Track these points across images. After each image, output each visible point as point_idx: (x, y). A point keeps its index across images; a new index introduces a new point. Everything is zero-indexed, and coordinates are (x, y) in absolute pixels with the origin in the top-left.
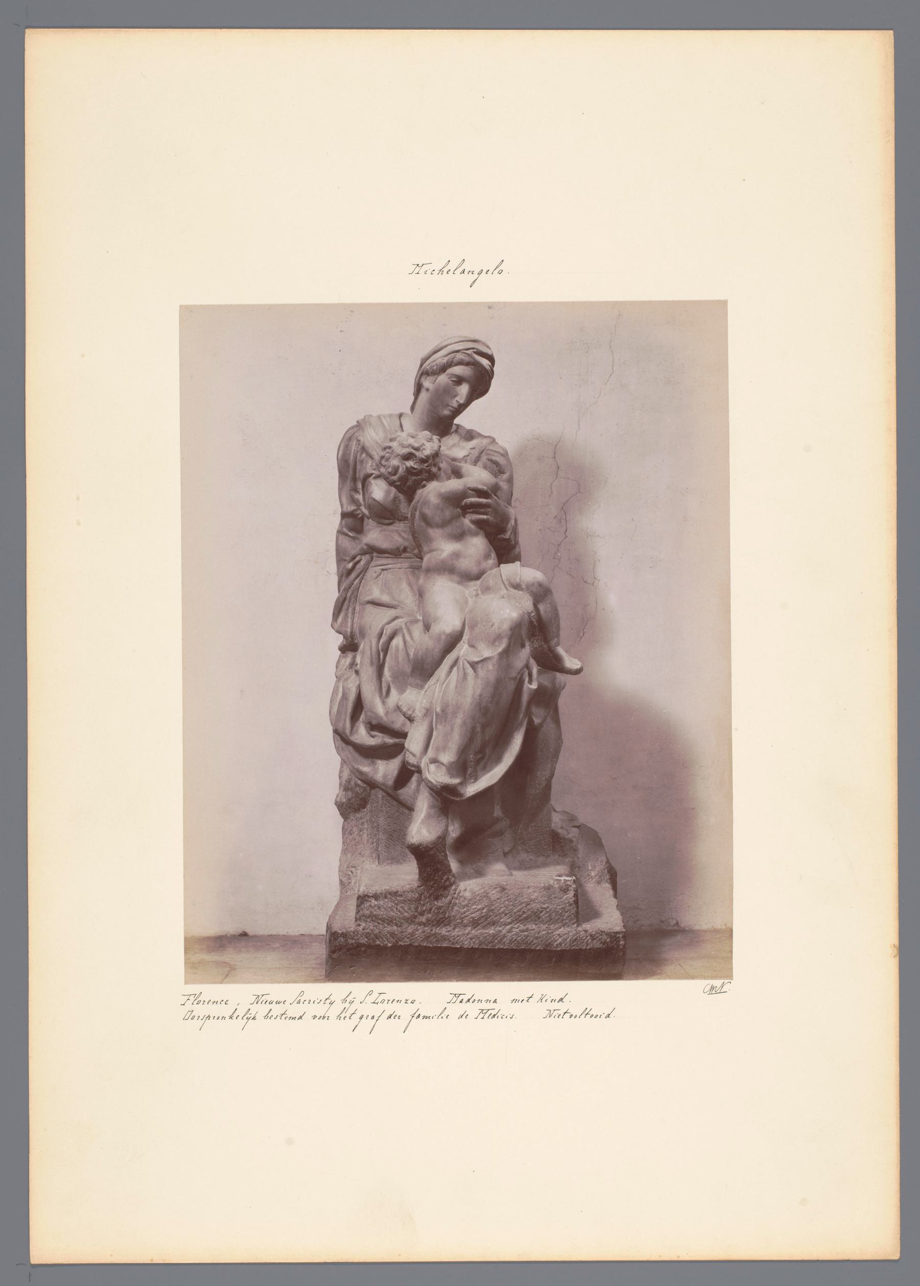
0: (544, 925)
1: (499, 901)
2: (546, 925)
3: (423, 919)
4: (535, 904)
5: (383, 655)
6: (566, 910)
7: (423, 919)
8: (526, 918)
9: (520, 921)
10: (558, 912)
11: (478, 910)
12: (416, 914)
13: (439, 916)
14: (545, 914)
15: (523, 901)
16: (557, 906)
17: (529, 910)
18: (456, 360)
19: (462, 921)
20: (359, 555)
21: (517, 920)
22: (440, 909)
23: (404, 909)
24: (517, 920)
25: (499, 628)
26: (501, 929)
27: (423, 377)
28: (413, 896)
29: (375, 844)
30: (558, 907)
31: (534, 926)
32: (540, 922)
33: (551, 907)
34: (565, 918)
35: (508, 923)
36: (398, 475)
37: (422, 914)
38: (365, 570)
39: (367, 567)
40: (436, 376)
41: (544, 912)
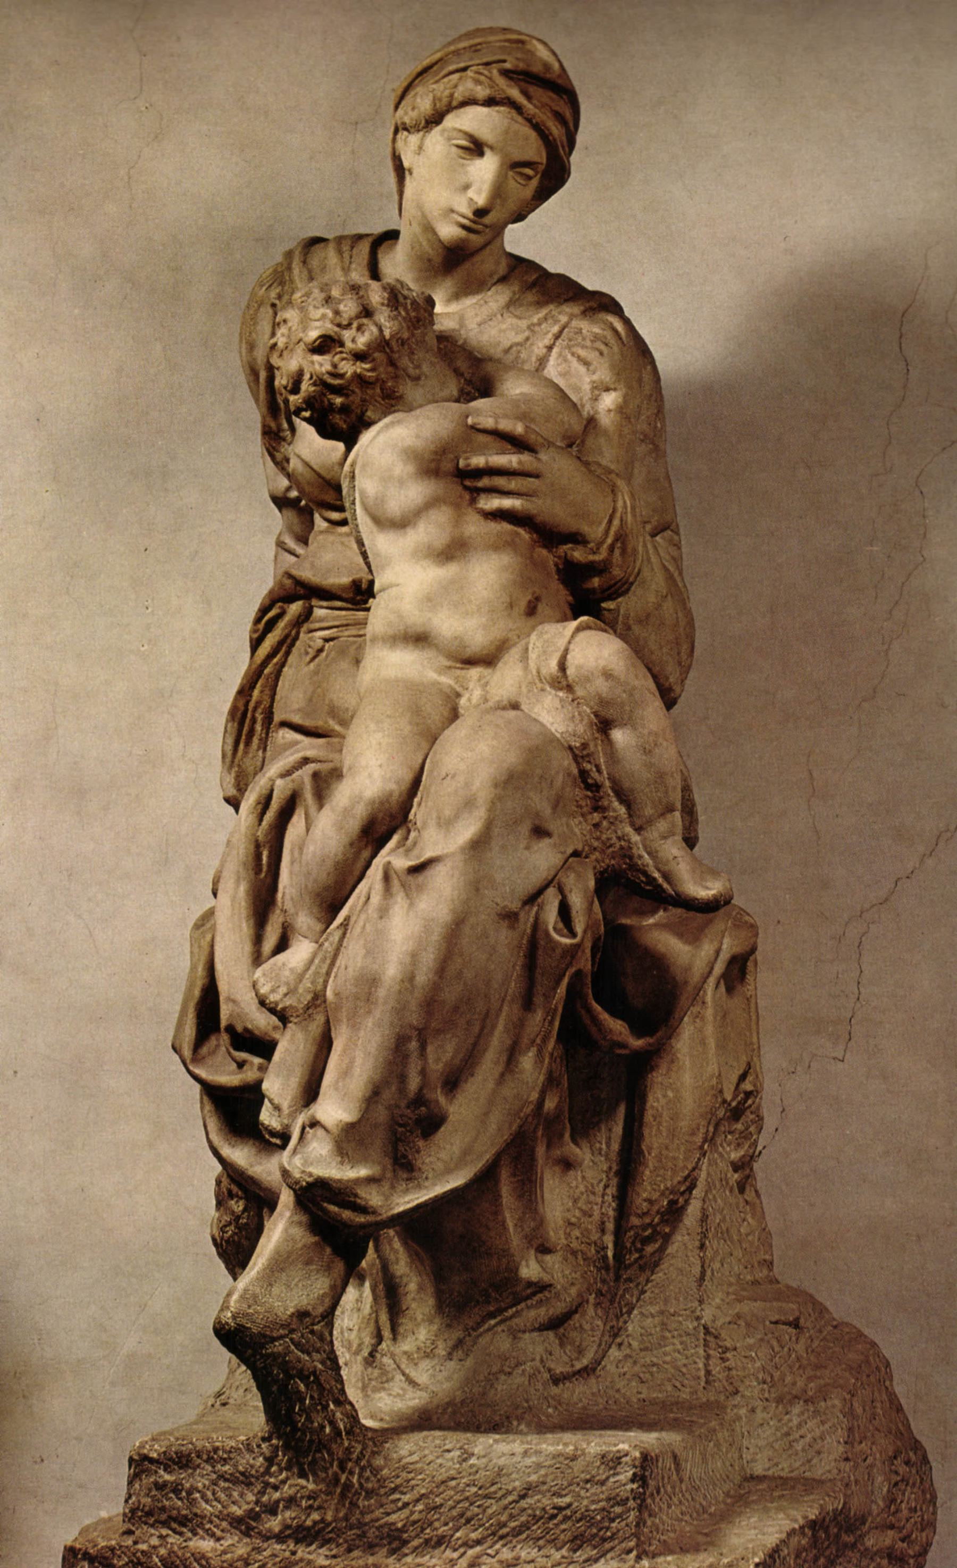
0: (558, 1549)
1: (453, 1483)
2: (564, 1552)
3: (274, 1524)
4: (539, 1497)
5: (269, 857)
6: (612, 1515)
7: (274, 1524)
8: (517, 1532)
9: (502, 1538)
10: (593, 1518)
11: (406, 1505)
12: (258, 1509)
13: (312, 1517)
14: (562, 1522)
15: (510, 1488)
16: (593, 1502)
17: (525, 1509)
18: (458, 96)
19: (364, 1533)
20: (278, 601)
21: (494, 1534)
22: (315, 1499)
23: (230, 1496)
24: (494, 1534)
25: (467, 785)
26: (455, 1555)
27: (399, 136)
28: (252, 1461)
29: (526, 1405)
30: (593, 1507)
31: (534, 1553)
32: (549, 1542)
33: (576, 1504)
34: (609, 1534)
35: (473, 1541)
36: (303, 394)
37: (272, 1510)
38: (289, 641)
39: (294, 632)
40: (421, 133)
41: (560, 1517)
